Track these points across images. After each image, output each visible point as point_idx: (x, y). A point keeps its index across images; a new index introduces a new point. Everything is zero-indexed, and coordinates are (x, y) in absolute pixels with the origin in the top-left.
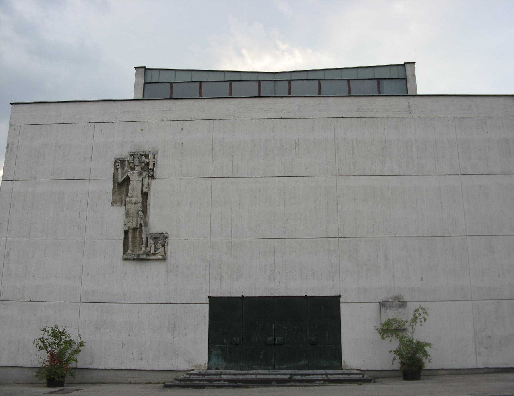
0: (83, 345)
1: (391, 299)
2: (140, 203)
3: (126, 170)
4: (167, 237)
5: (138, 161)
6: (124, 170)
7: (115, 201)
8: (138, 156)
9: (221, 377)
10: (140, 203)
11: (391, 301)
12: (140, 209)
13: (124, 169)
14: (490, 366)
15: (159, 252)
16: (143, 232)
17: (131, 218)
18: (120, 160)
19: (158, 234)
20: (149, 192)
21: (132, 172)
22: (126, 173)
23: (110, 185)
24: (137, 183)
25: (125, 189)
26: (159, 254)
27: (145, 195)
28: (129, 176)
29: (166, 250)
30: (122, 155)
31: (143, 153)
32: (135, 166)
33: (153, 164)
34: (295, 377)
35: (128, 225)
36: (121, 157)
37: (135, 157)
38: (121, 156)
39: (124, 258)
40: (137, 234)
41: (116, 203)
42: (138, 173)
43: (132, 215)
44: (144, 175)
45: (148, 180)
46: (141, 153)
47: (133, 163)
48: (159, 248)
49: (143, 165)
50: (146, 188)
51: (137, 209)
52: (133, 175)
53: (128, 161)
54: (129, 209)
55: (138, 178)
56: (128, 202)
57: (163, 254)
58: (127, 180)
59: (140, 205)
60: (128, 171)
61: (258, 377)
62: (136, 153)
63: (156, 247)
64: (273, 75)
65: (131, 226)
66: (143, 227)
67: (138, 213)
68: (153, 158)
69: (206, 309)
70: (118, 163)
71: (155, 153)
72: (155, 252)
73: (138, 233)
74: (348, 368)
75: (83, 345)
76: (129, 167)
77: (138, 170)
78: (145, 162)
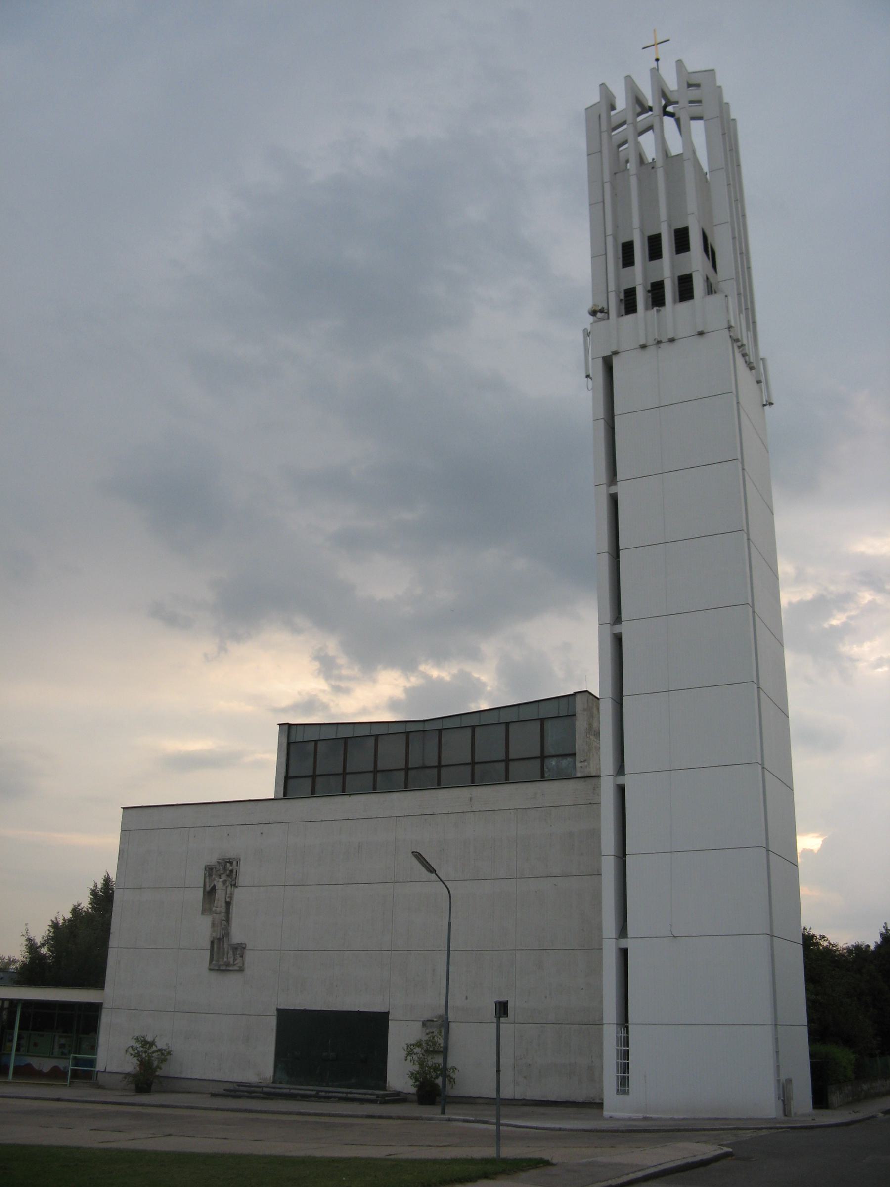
0: (170, 1055)
1: (436, 1018)
9: (262, 1090)
11: (435, 1020)
12: (224, 919)
14: (528, 1098)
23: (200, 894)
27: (228, 904)
31: (228, 860)
34: (320, 1093)
44: (228, 883)
49: (228, 872)
50: (229, 897)
57: (240, 965)
58: (214, 889)
59: (223, 914)
61: (292, 1091)
64: (422, 723)
69: (273, 1022)
74: (391, 1090)
75: (170, 1055)
77: (224, 877)
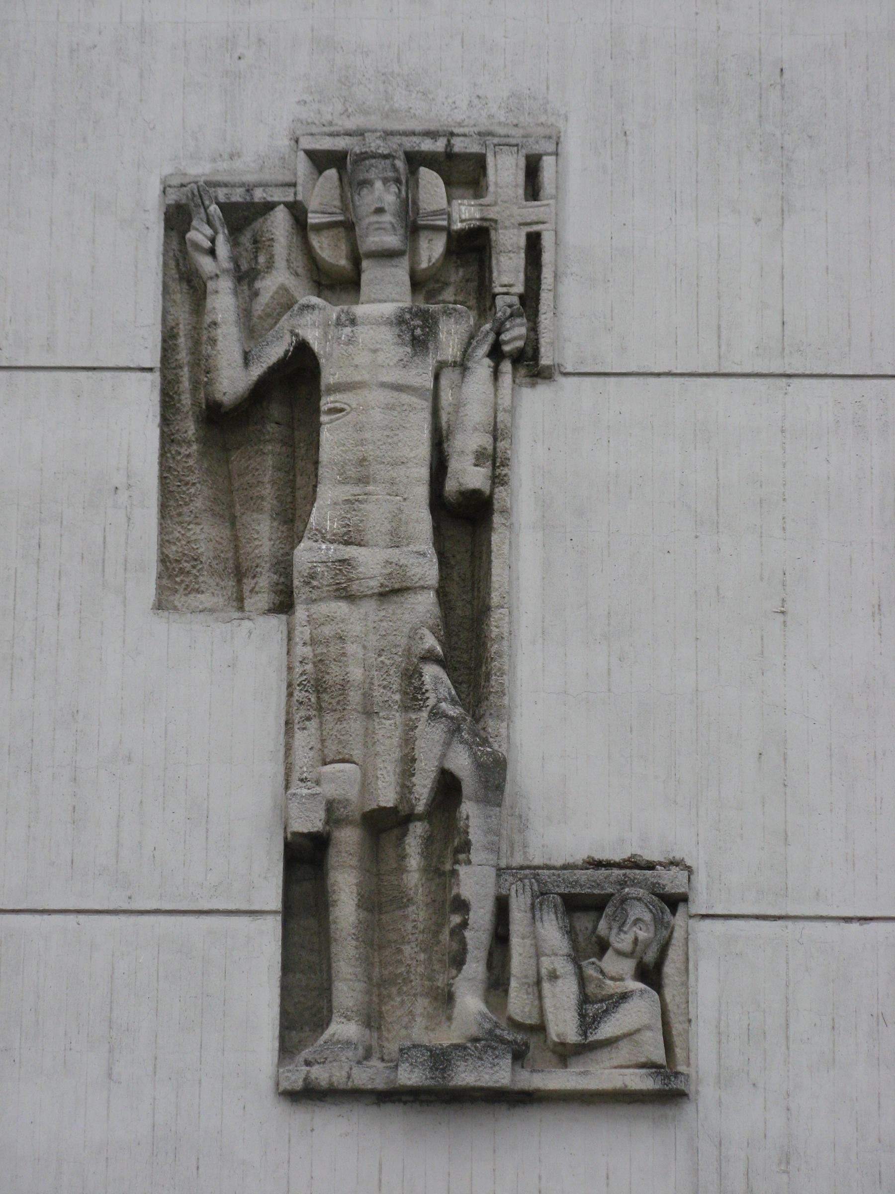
2: (423, 588)
3: (283, 289)
4: (684, 899)
5: (397, 214)
6: (256, 294)
7: (182, 571)
8: (395, 169)
10: (423, 588)
12: (430, 642)
13: (258, 284)
15: (618, 1032)
16: (466, 847)
17: (355, 725)
18: (222, 198)
19: (603, 872)
20: (500, 493)
21: (334, 312)
22: (285, 322)
24: (390, 407)
25: (270, 462)
26: (624, 1047)
28: (316, 347)
29: (671, 1007)
30: (231, 157)
31: (427, 145)
32: (356, 259)
33: (522, 242)
35: (329, 790)
36: (223, 170)
37: (372, 175)
38: (224, 165)
39: (299, 1085)
40: (401, 870)
41: (190, 590)
42: (400, 321)
43: (355, 697)
45: (489, 388)
46: (411, 143)
47: (341, 232)
48: (624, 997)
50: (480, 457)
51: (403, 641)
52: (350, 341)
53: (298, 212)
54: (327, 643)
55: (404, 365)
56: (312, 576)
60: (303, 301)
62: (375, 144)
63: (591, 989)
65: (353, 793)
66: (468, 808)
67: (411, 675)
68: (521, 191)
70: (209, 223)
71: (537, 149)
72: (585, 1034)
73: (414, 861)
76: (300, 264)
78: (447, 230)
